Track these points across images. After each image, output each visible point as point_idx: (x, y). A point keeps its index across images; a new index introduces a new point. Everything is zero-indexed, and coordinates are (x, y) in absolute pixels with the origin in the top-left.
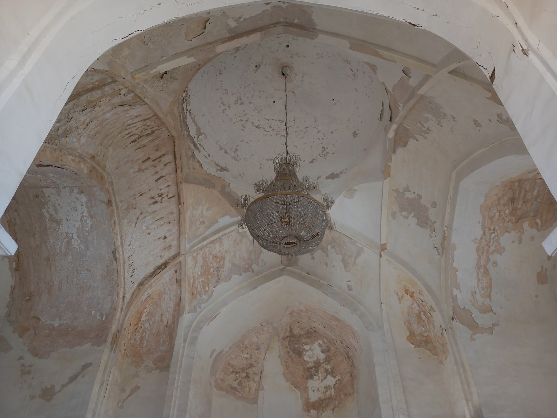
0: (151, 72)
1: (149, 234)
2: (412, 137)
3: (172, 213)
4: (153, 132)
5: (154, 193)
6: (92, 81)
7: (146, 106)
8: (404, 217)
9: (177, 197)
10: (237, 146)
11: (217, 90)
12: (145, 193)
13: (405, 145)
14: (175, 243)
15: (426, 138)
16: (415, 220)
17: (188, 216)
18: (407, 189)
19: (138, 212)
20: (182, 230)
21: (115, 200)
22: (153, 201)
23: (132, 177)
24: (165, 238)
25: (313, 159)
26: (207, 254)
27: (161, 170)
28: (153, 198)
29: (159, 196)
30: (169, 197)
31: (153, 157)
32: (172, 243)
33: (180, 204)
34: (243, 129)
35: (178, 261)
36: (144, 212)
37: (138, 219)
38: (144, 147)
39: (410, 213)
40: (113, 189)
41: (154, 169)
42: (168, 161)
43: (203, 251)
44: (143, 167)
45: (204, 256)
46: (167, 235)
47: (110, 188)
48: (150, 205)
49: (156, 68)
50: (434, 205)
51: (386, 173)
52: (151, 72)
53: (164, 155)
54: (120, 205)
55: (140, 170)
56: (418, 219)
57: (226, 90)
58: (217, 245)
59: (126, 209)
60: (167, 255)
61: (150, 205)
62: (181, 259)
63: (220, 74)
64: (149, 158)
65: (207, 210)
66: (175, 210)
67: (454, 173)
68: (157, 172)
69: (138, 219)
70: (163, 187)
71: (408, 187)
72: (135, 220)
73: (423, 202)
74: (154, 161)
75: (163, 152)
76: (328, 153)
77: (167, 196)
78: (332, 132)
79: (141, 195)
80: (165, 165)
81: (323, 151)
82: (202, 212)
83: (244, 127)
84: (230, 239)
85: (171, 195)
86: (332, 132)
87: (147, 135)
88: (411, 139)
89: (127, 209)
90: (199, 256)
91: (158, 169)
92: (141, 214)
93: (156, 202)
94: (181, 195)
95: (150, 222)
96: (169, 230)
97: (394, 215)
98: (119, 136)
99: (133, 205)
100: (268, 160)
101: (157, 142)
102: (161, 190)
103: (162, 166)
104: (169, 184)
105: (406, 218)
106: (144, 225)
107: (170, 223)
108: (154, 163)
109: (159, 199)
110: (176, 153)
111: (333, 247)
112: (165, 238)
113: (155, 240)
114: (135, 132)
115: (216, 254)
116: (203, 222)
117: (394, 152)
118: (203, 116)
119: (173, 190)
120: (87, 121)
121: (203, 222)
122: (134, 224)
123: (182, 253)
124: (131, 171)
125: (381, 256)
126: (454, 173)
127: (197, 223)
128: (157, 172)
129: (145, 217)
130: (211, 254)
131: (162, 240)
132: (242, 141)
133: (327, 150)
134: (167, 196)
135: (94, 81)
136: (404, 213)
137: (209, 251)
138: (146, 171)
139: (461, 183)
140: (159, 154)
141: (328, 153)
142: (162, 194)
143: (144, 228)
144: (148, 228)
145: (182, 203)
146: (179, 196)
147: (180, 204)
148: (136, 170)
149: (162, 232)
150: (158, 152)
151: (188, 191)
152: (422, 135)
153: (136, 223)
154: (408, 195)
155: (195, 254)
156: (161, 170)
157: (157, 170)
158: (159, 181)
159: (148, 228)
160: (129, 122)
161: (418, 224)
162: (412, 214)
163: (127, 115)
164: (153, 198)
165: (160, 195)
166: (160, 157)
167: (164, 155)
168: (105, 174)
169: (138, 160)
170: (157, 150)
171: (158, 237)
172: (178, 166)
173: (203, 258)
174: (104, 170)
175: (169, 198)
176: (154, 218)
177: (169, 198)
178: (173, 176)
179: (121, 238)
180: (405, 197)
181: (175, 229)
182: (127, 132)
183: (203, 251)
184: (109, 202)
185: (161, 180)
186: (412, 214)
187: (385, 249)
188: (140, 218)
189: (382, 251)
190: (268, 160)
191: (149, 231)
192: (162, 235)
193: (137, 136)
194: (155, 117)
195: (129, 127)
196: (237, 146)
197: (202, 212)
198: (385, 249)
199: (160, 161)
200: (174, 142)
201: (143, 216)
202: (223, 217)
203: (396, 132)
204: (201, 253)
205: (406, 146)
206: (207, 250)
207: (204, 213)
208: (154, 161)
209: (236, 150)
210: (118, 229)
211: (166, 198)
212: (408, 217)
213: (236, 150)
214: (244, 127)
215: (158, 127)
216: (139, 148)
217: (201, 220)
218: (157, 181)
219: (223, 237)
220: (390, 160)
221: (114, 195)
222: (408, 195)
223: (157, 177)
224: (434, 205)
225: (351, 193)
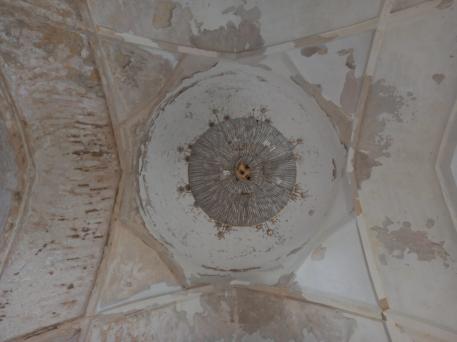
0: (116, 34)
1: (51, 273)
2: (373, 165)
3: (92, 257)
4: (100, 154)
5: (79, 224)
6: (57, 7)
7: (103, 100)
8: (398, 257)
9: (105, 238)
10: (187, 234)
11: (174, 176)
12: (68, 220)
13: (368, 176)
14: (82, 299)
15: (388, 155)
16: (414, 255)
17: (112, 266)
18: (389, 222)
19: (48, 237)
20: (99, 280)
21: (27, 201)
22: (74, 233)
23: (60, 193)
24: (71, 287)
25: (270, 248)
26: (125, 334)
27: (97, 202)
28: (75, 230)
29: (84, 231)
30: (96, 235)
31: (92, 185)
32: (78, 298)
33: (106, 245)
34: (195, 220)
35: (76, 327)
36: (57, 242)
37: (45, 246)
38: (87, 171)
39: (403, 250)
40: (30, 188)
41: (90, 198)
42: (108, 197)
43: (120, 326)
44: (78, 190)
45: (118, 334)
46: (75, 284)
47: (28, 184)
48: (68, 236)
49: (121, 33)
50: (430, 223)
51: (355, 209)
52: (116, 34)
53: (105, 188)
54: (30, 213)
55: (72, 192)
56: (417, 252)
57: (182, 179)
58: (142, 322)
59: (35, 224)
60: (65, 314)
61: (68, 236)
62: (84, 323)
63: (179, 161)
64: (88, 185)
65: (139, 270)
66: (98, 254)
67: (437, 168)
68: (91, 203)
69: (45, 246)
70: (92, 221)
71: (388, 219)
72: (40, 246)
73: (414, 228)
74: (92, 190)
75: (105, 185)
76: (285, 239)
77: (94, 233)
78: (287, 221)
79: (62, 220)
80: (103, 199)
81: (280, 240)
82: (132, 270)
83: (196, 218)
84: (162, 318)
85: (98, 234)
86: (287, 221)
87: (94, 154)
88: (373, 167)
89: (37, 224)
90: (112, 333)
91: (93, 200)
92: (52, 242)
93: (77, 236)
94: (111, 234)
95: (60, 258)
96: (81, 278)
97: (383, 259)
98: (64, 130)
99: (47, 225)
100: (219, 251)
101: (102, 173)
102: (89, 224)
103: (99, 198)
104: (100, 221)
105: (401, 257)
106: (49, 258)
107: (85, 268)
108: (91, 192)
109: (82, 234)
110: (119, 191)
111: (311, 330)
112: (71, 287)
113: (55, 286)
114: (81, 138)
115: (137, 337)
116: (130, 284)
117: (359, 187)
118: (156, 194)
119: (103, 229)
120: (37, 71)
121: (130, 284)
122: (36, 250)
123: (88, 314)
124: (61, 187)
125: (384, 318)
126: (437, 168)
127: (122, 282)
128: (91, 203)
129: (55, 249)
130: (129, 334)
131: (65, 289)
132: (193, 231)
133: (284, 238)
134: (94, 233)
135: (60, 8)
136: (396, 253)
137: (128, 329)
138: (79, 196)
139: (452, 166)
140: (100, 185)
141: (285, 239)
142: (88, 230)
143: (48, 263)
144: (53, 265)
145: (109, 244)
146: (108, 235)
147: (106, 245)
148: (68, 189)
149: (69, 278)
150: (100, 183)
151: (121, 236)
152: (383, 154)
153: (40, 250)
154: (391, 228)
155: (105, 328)
156: (97, 202)
157: (91, 201)
158: (89, 213)
159: (53, 265)
160: (80, 118)
161: (420, 259)
162: (408, 250)
163: (80, 105)
164: (75, 230)
165: (86, 230)
166: (100, 189)
167: (105, 188)
168: (29, 161)
169: (75, 180)
170: (99, 181)
171: (61, 283)
172: (118, 201)
173: (117, 338)
174: (31, 156)
175: (95, 237)
176: (66, 255)
177: (95, 237)
178: (108, 213)
179: (9, 253)
180: (389, 233)
181: (89, 279)
182: (73, 131)
183: (120, 326)
184: (18, 196)
185: (92, 213)
186: (408, 250)
187: (388, 308)
188: (48, 247)
189: (384, 309)
190: (219, 251)
191: (52, 269)
192: (68, 282)
193: (82, 148)
194: (106, 130)
195: (77, 125)
196: (187, 234)
197: (132, 270)
198: (388, 308)
199: (99, 193)
200: (121, 177)
201: (53, 246)
202: (157, 283)
203: (355, 162)
204: (116, 329)
205: (370, 177)
206: (125, 326)
207: (135, 272)
208: (92, 190)
209: (185, 237)
210: (11, 239)
211: (91, 236)
212: (403, 255)
213: (185, 237)
214: (196, 218)
215: (109, 148)
216: (81, 169)
217: (128, 280)
218: (87, 212)
219: (153, 313)
220: (356, 195)
221: (29, 195)
222: (391, 228)
223: (88, 208)
224: (430, 223)
225: (320, 251)
